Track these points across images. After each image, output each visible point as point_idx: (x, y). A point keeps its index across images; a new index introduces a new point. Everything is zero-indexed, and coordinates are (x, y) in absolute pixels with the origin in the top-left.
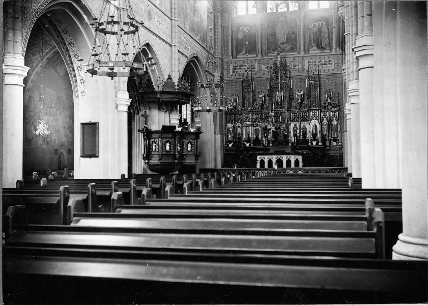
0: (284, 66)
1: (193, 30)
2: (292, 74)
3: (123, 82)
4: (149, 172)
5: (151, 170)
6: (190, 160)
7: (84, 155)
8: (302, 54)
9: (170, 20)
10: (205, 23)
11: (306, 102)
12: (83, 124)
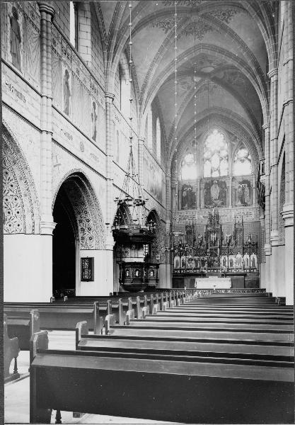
0: (218, 217)
1: (152, 191)
2: (223, 222)
3: (47, 206)
4: (123, 291)
5: (125, 289)
6: (152, 283)
7: (83, 280)
8: (230, 207)
9: (39, 97)
10: (160, 186)
11: (233, 241)
12: (82, 259)
